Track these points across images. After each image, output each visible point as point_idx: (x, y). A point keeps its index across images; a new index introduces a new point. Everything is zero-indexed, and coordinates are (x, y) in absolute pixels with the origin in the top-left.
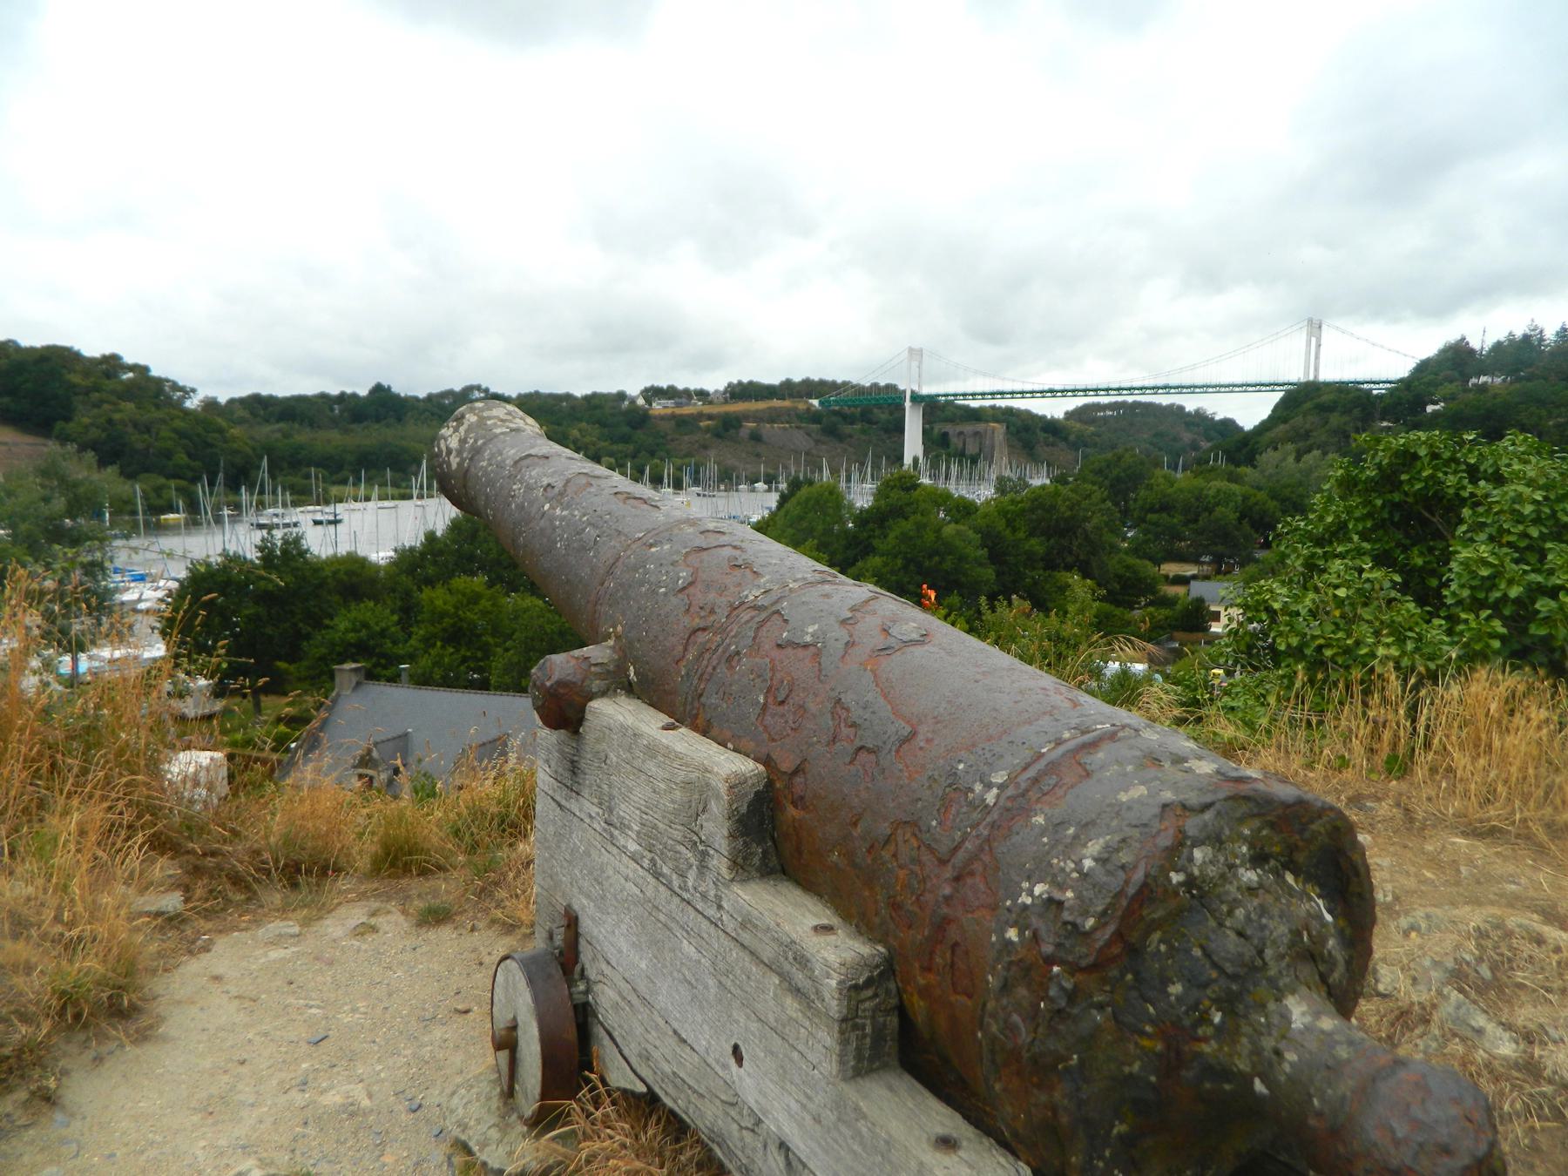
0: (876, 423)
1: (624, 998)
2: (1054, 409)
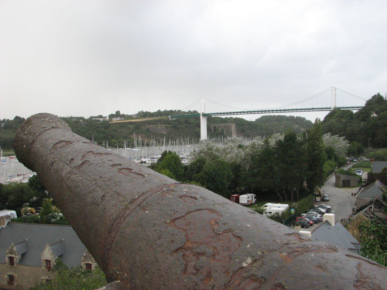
1: (247, 268)
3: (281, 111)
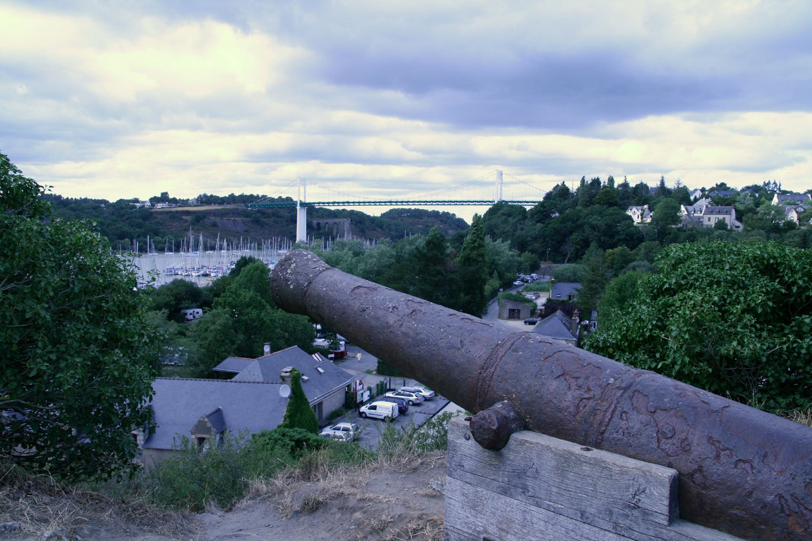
0: (281, 217)
2: (375, 212)
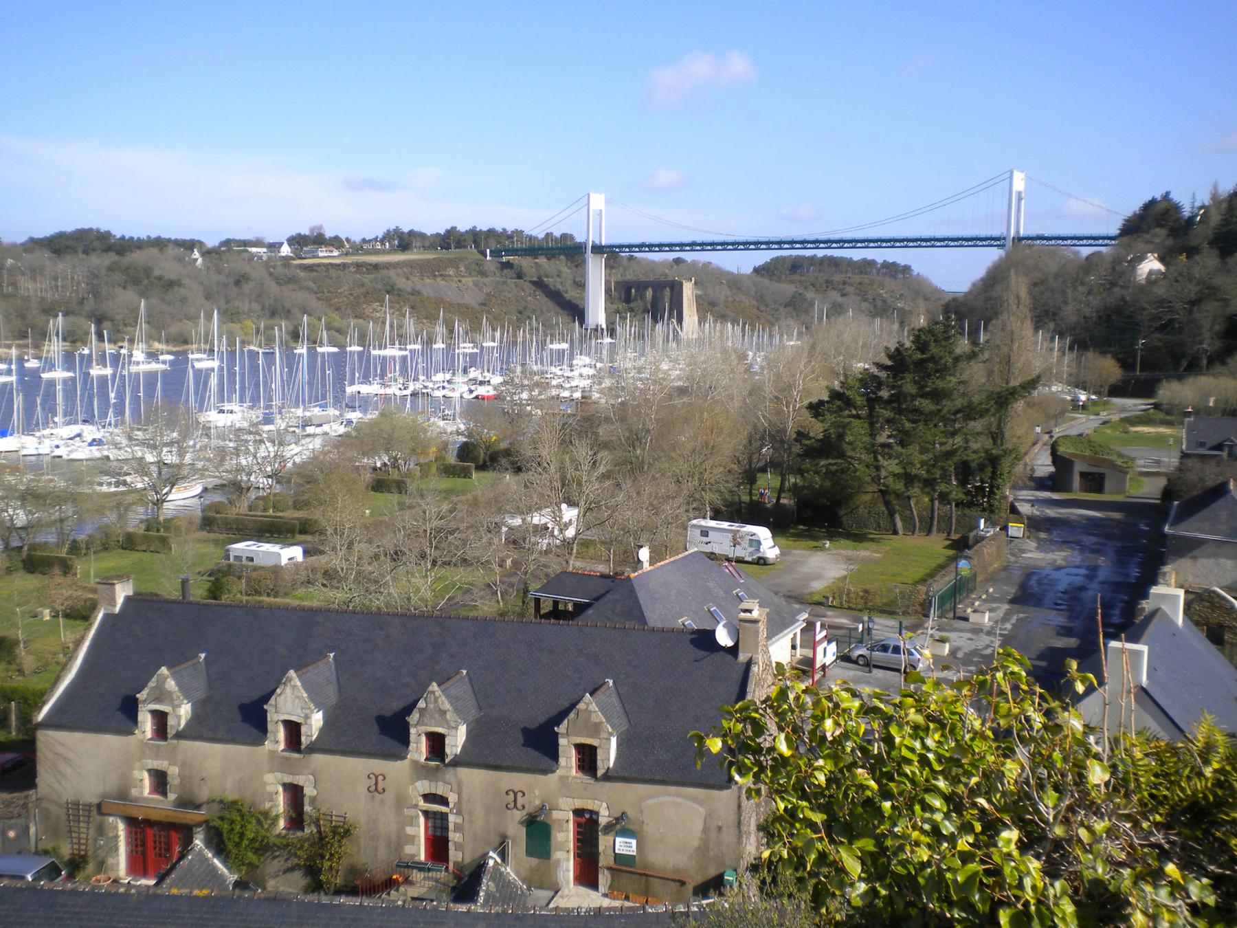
3: (829, 243)
